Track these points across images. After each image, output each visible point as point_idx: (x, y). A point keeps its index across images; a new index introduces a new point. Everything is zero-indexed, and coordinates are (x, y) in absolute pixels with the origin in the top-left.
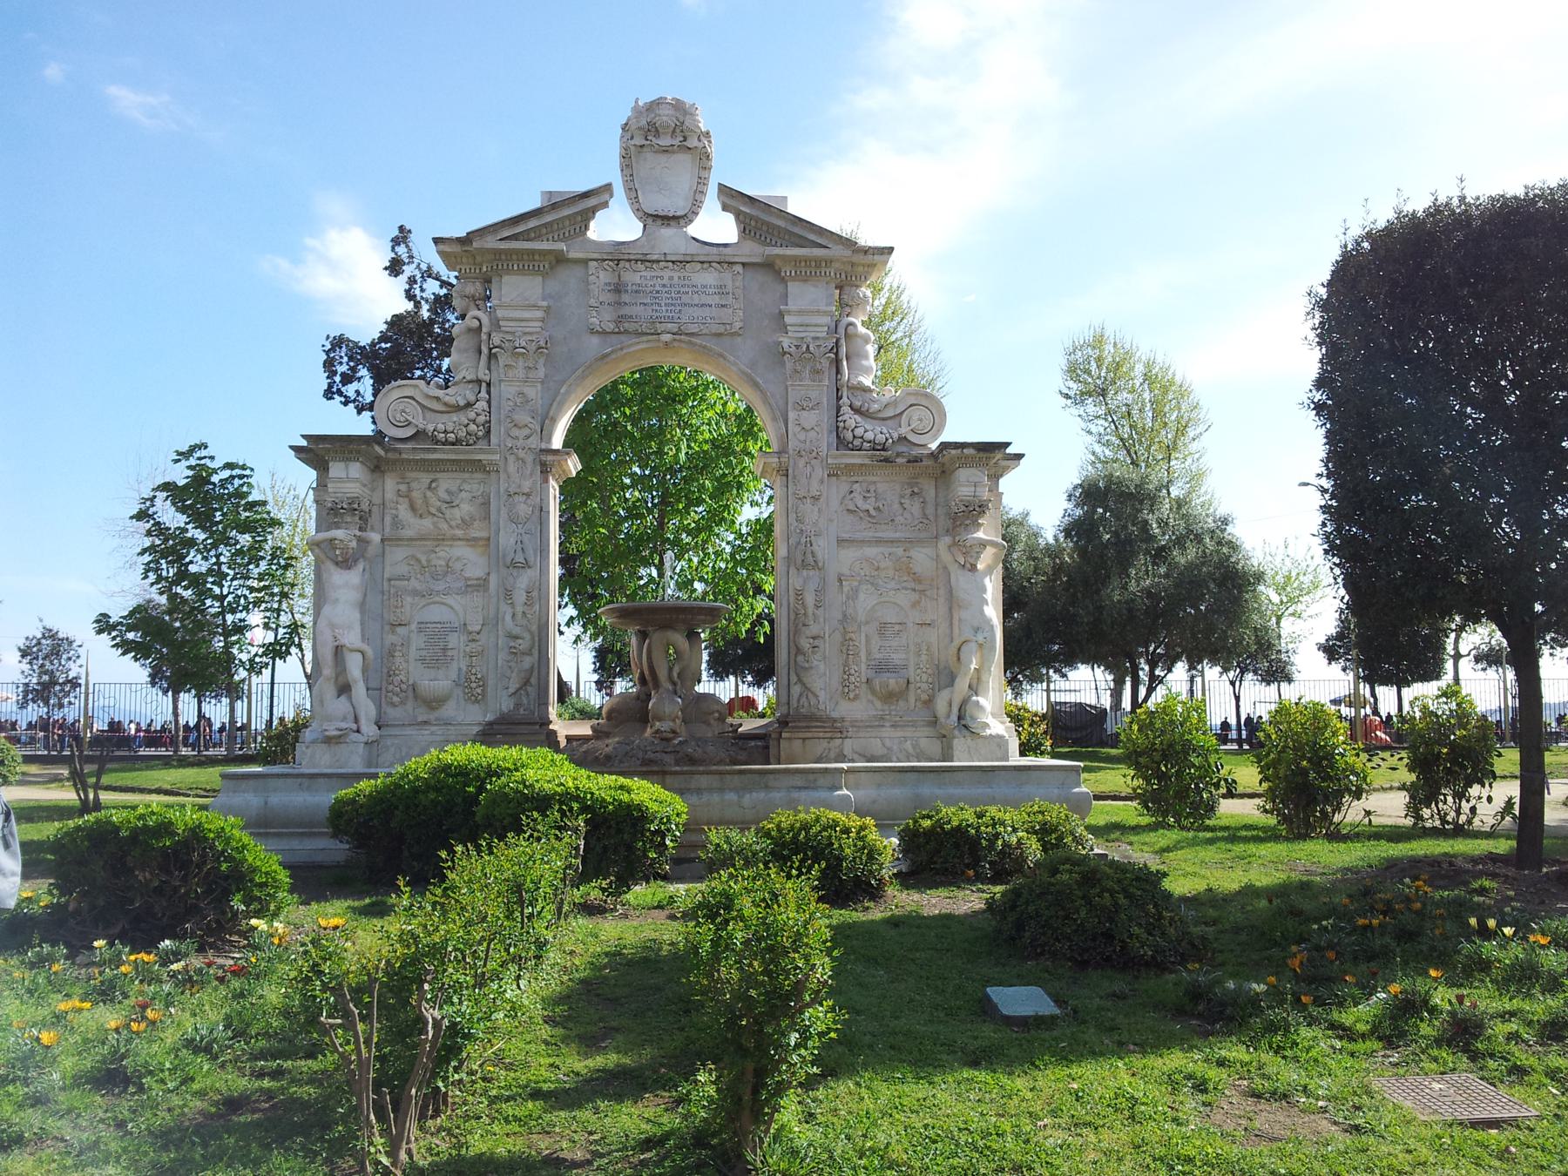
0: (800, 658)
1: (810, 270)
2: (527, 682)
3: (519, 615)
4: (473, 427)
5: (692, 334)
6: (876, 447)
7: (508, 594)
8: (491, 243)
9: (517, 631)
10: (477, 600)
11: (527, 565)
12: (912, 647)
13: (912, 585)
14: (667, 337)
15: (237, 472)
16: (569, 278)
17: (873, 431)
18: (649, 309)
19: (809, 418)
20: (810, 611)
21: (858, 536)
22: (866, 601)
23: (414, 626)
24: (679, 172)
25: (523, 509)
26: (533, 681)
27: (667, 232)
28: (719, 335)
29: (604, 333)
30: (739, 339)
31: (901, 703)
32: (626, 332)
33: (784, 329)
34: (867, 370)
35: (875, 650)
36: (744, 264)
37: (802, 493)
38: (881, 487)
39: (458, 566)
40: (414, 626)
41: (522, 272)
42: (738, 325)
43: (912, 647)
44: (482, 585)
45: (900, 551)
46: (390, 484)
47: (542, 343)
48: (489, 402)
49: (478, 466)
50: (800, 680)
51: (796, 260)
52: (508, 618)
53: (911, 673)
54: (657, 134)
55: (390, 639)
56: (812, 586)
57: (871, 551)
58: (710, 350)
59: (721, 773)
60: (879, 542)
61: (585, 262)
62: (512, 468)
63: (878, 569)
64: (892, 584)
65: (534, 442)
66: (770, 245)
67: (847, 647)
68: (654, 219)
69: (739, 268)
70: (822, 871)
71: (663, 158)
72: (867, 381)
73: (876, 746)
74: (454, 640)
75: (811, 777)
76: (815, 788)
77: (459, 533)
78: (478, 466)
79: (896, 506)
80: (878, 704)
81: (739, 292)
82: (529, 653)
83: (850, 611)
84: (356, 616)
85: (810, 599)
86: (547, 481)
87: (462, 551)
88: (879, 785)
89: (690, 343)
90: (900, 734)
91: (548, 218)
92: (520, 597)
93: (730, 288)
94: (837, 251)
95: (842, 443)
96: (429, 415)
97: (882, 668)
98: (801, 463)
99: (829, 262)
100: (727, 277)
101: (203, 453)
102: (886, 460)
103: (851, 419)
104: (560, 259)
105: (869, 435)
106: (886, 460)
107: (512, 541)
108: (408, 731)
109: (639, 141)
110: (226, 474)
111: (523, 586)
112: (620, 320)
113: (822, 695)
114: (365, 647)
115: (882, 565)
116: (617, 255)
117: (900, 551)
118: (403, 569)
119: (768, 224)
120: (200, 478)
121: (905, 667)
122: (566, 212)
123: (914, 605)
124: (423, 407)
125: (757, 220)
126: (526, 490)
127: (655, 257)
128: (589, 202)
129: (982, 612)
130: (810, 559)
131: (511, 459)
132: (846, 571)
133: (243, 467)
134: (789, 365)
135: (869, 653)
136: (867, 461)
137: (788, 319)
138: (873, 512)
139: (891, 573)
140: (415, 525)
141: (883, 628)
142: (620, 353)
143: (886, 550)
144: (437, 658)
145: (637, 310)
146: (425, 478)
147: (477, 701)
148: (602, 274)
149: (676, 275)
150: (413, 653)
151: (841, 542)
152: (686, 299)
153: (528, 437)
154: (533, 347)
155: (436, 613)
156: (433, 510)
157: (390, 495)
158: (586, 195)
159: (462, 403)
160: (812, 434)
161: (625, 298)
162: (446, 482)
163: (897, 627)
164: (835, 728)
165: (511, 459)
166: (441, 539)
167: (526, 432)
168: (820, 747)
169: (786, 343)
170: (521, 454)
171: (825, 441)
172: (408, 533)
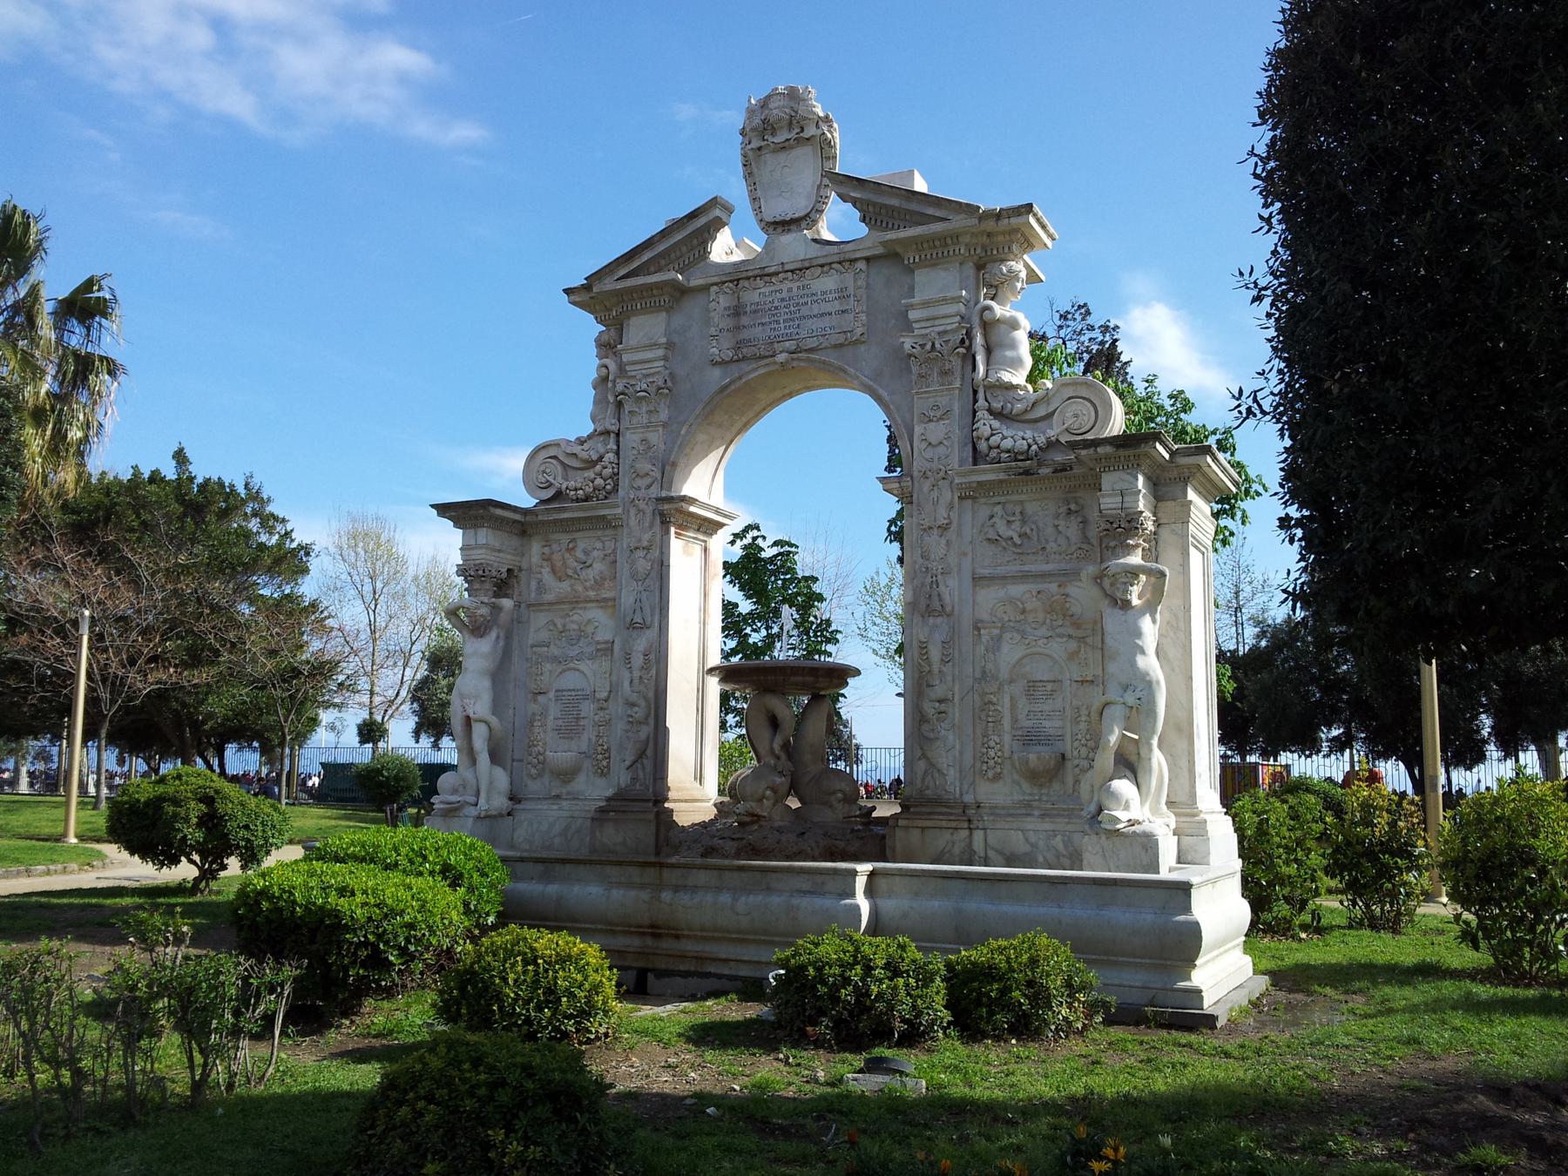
0: (925, 727)
1: (936, 251)
2: (641, 755)
3: (636, 681)
4: (599, 481)
5: (811, 350)
6: (1015, 455)
7: (627, 658)
8: (609, 284)
9: (634, 697)
10: (605, 664)
11: (644, 626)
12: (1069, 713)
13: (1071, 631)
14: (782, 358)
15: (787, 548)
16: (693, 307)
17: (1014, 438)
18: (767, 328)
19: (936, 431)
20: (936, 670)
21: (1000, 571)
22: (1010, 652)
23: (552, 695)
24: (801, 172)
25: (643, 565)
26: (649, 752)
27: (786, 239)
28: (841, 345)
29: (723, 363)
30: (862, 348)
31: (1056, 786)
32: (744, 358)
33: (908, 326)
34: (1016, 363)
35: (1022, 717)
36: (868, 259)
37: (926, 523)
38: (1031, 508)
39: (590, 629)
40: (552, 695)
41: (646, 310)
42: (859, 331)
43: (1069, 713)
44: (607, 649)
45: (1053, 587)
46: (536, 548)
47: (661, 383)
48: (617, 453)
49: (604, 523)
50: (924, 756)
51: (917, 242)
52: (626, 684)
53: (1067, 747)
54: (774, 133)
55: (533, 708)
56: (938, 637)
57: (1016, 590)
58: (830, 364)
59: (720, 869)
60: (1024, 577)
61: (705, 288)
62: (633, 522)
63: (1023, 612)
64: (1043, 631)
65: (655, 492)
66: (886, 229)
67: (985, 711)
68: (778, 226)
69: (861, 265)
70: (1021, 1004)
71: (782, 156)
72: (1018, 377)
73: (1018, 843)
74: (587, 709)
75: (819, 879)
76: (823, 894)
77: (592, 594)
78: (604, 523)
79: (1050, 530)
80: (1026, 786)
81: (862, 292)
82: (645, 722)
83: (990, 666)
84: (486, 683)
85: (935, 653)
86: (668, 532)
87: (596, 614)
88: (916, 894)
89: (809, 360)
90: (1047, 826)
91: (661, 247)
92: (638, 660)
93: (851, 290)
94: (958, 222)
95: (977, 457)
96: (571, 473)
97: (1029, 739)
98: (926, 486)
99: (956, 237)
100: (849, 278)
101: (756, 533)
102: (1027, 472)
103: (986, 424)
104: (681, 292)
105: (1008, 443)
106: (1027, 472)
107: (632, 600)
108: (543, 806)
109: (756, 144)
110: (775, 550)
111: (641, 648)
112: (738, 347)
113: (952, 774)
114: (494, 720)
115: (1028, 607)
116: (737, 276)
117: (1053, 587)
118: (544, 635)
119: (882, 206)
120: (752, 552)
121: (1061, 738)
122: (678, 237)
123: (1072, 656)
124: (562, 463)
125: (875, 204)
126: (645, 544)
127: (772, 270)
128: (699, 225)
129: (1133, 664)
130: (936, 604)
131: (633, 512)
132: (986, 617)
133: (791, 545)
134: (915, 369)
135: (1015, 720)
136: (1002, 476)
137: (912, 315)
138: (1017, 540)
139: (1041, 616)
140: (557, 588)
141: (1032, 687)
142: (739, 383)
143: (1033, 587)
144: (570, 730)
145: (757, 332)
146: (564, 538)
147: (603, 774)
148: (722, 299)
149: (794, 286)
150: (550, 723)
151: (977, 580)
152: (805, 311)
153: (649, 487)
154: (652, 390)
155: (571, 681)
156: (570, 572)
157: (535, 559)
158: (693, 215)
159: (595, 457)
160: (941, 450)
161: (745, 320)
162: (585, 541)
163: (1049, 687)
164: (967, 815)
165: (633, 512)
166: (575, 602)
167: (647, 481)
168: (942, 840)
169: (908, 343)
170: (642, 505)
171: (955, 457)
172: (549, 597)
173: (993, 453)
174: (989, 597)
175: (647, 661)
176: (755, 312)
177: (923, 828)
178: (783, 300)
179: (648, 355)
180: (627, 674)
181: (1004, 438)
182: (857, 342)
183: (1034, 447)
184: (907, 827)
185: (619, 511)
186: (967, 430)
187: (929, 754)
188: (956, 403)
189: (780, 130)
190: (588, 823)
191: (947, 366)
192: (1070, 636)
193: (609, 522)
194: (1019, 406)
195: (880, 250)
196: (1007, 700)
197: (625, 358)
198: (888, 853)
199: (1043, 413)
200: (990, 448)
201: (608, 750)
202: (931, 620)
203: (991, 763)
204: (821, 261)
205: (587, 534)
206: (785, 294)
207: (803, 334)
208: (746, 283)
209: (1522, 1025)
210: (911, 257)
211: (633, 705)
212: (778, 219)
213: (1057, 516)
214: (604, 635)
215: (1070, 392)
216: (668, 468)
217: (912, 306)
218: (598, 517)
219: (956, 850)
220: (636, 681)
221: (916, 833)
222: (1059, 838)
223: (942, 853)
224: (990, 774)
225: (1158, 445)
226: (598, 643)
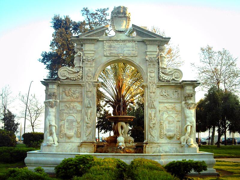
3: (89, 118)
17: (167, 78)
18: (117, 51)
19: (153, 75)
21: (163, 101)
22: (165, 116)
30: (137, 57)
36: (138, 41)
42: (136, 54)
51: (149, 40)
52: (86, 119)
56: (153, 112)
57: (166, 105)
64: (171, 112)
92: (89, 115)
98: (151, 84)
103: (162, 75)
107: (87, 102)
130: (153, 106)
131: (87, 84)
135: (166, 128)
146: (69, 88)
149: (123, 44)
153: (91, 79)
154: (92, 59)
155: (71, 118)
156: (70, 95)
161: (112, 49)
163: (172, 122)
167: (90, 78)
171: (156, 80)
173: (163, 80)
174: (162, 105)
176: (114, 47)
177: (151, 147)
178: (120, 46)
180: (87, 117)
181: (165, 78)
182: (136, 56)
183: (171, 80)
184: (148, 147)
185: (84, 83)
186: (158, 75)
187: (151, 134)
188: (156, 71)
191: (154, 63)
192: (176, 113)
193: (81, 85)
194: (167, 72)
195: (141, 40)
196: (165, 124)
197: (85, 52)
199: (171, 74)
200: (163, 79)
201: (80, 132)
202: (152, 109)
203: (162, 135)
204: (128, 40)
205: (73, 87)
206: (120, 45)
207: (125, 53)
209: (220, 173)
212: (119, 30)
213: (174, 92)
214: (79, 109)
215: (175, 71)
216: (95, 76)
217: (148, 52)
218: (79, 84)
219: (157, 151)
220: (89, 118)
221: (150, 148)
222: (174, 148)
223: (155, 152)
224: (162, 137)
226: (77, 110)
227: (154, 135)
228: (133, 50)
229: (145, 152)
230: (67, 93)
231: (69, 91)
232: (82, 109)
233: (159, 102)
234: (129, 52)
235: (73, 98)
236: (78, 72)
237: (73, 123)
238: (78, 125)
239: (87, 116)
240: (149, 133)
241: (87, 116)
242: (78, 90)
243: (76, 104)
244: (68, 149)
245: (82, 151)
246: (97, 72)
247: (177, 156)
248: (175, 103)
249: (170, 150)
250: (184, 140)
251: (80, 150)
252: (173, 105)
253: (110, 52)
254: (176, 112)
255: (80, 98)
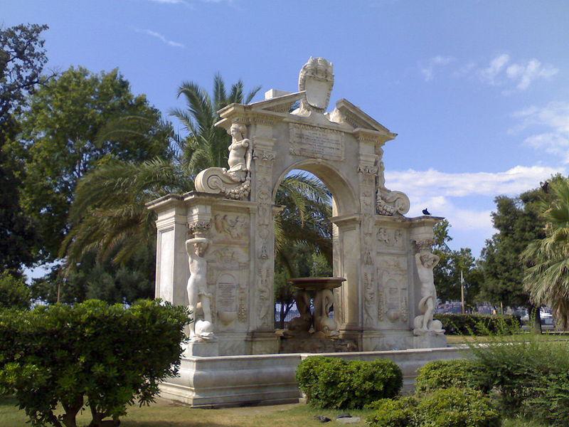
5: (326, 160)
9: (264, 289)
17: (390, 208)
51: (365, 134)
52: (260, 282)
57: (387, 258)
76: (423, 360)
95: (378, 212)
104: (280, 120)
116: (300, 121)
127: (315, 125)
130: (369, 260)
136: (389, 220)
161: (304, 141)
170: (265, 207)
173: (384, 212)
174: (380, 258)
175: (268, 273)
177: (371, 338)
179: (268, 143)
184: (366, 338)
189: (320, 75)
190: (243, 342)
198: (360, 348)
208: (329, 131)
210: (361, 137)
211: (262, 292)
225: (148, 208)
227: (371, 315)
228: (338, 149)
229: (362, 348)
230: (220, 225)
231: (224, 222)
232: (249, 261)
233: (378, 253)
234: (332, 151)
235: (230, 236)
236: (242, 182)
237: (232, 291)
238: (243, 294)
239: (261, 276)
240: (364, 311)
241: (261, 276)
242: (243, 217)
243: (237, 249)
244: (226, 348)
245: (258, 350)
246: (207, 197)
247: (446, 353)
248: (398, 255)
249: (396, 342)
250: (422, 323)
251: (252, 349)
252: (395, 258)
253: (299, 148)
254: (401, 273)
255: (244, 237)
